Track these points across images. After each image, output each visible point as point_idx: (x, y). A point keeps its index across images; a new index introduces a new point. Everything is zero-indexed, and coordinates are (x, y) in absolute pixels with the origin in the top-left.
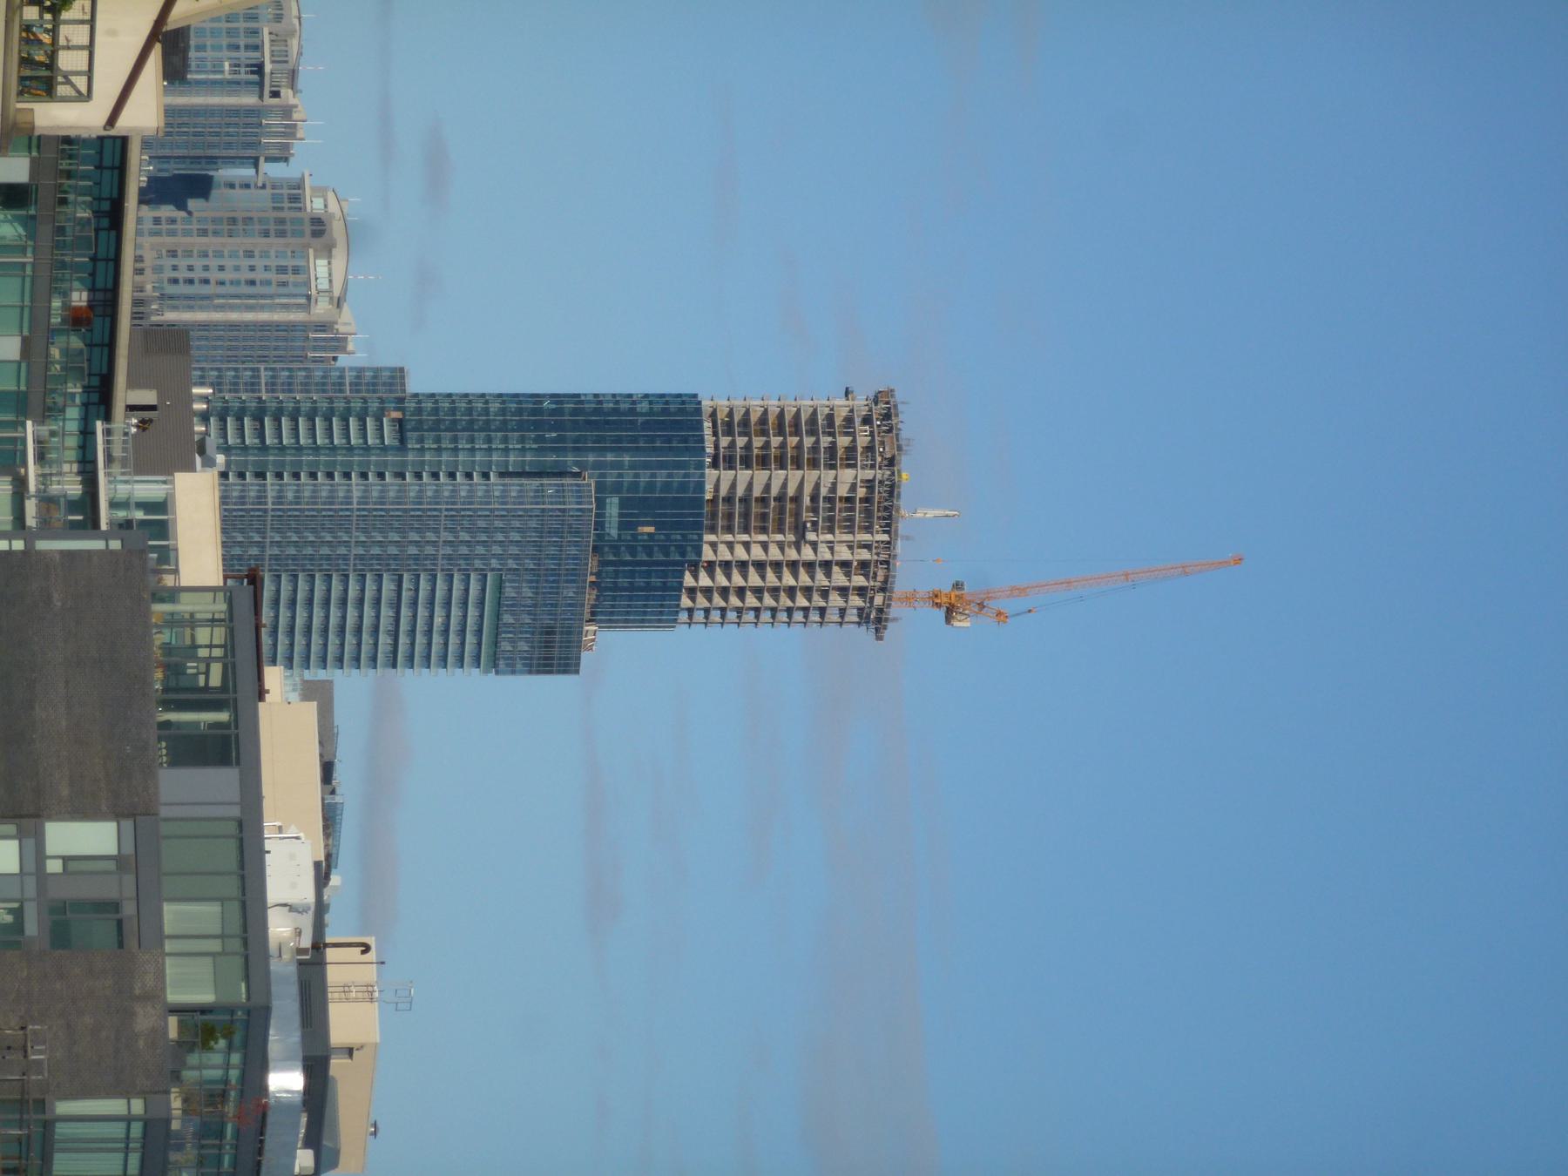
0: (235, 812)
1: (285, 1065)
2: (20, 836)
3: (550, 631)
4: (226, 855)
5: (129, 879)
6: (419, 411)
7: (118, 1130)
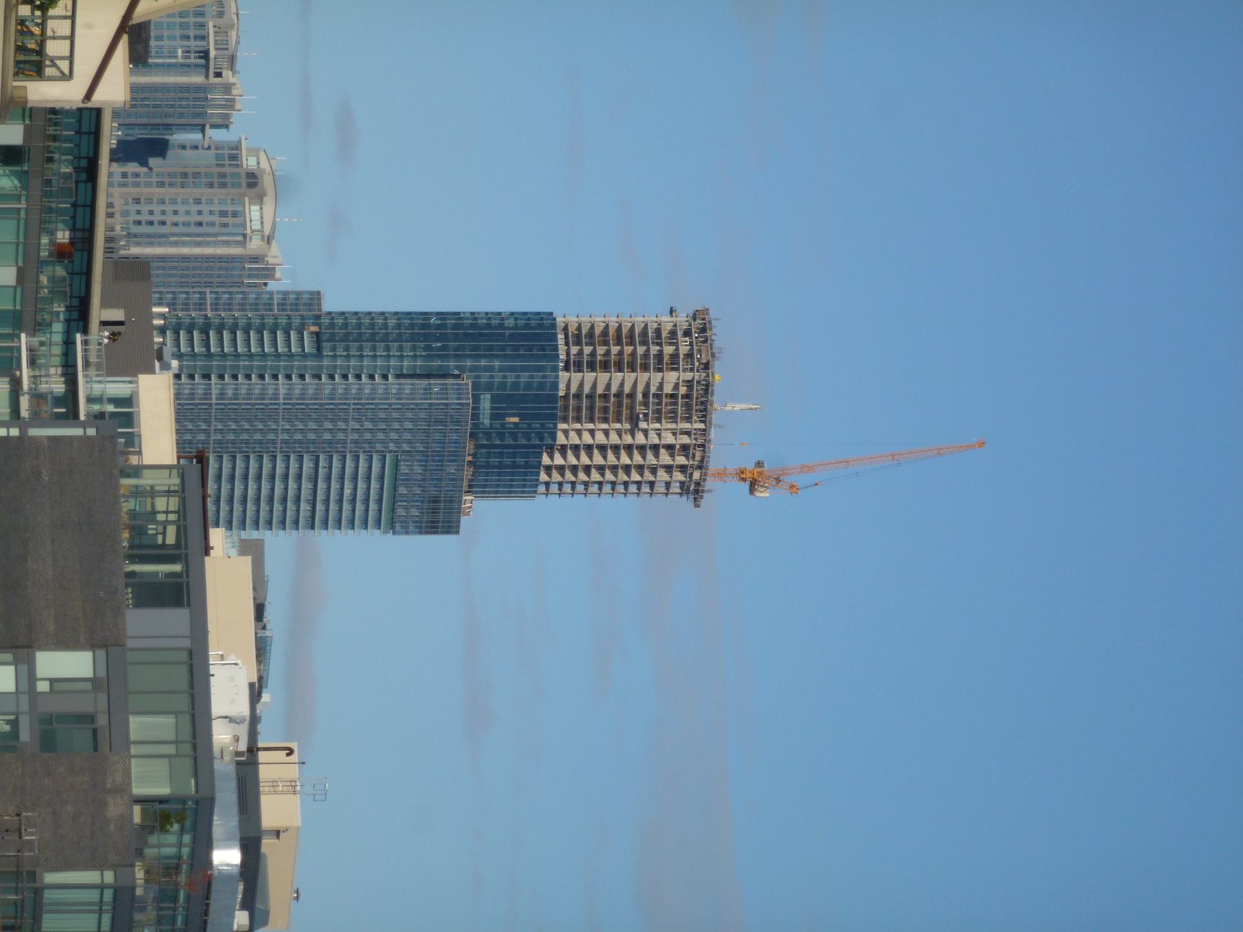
0: (186, 643)
1: (226, 844)
2: (16, 662)
3: (436, 500)
4: (179, 678)
5: (102, 697)
6: (332, 326)
7: (94, 895)
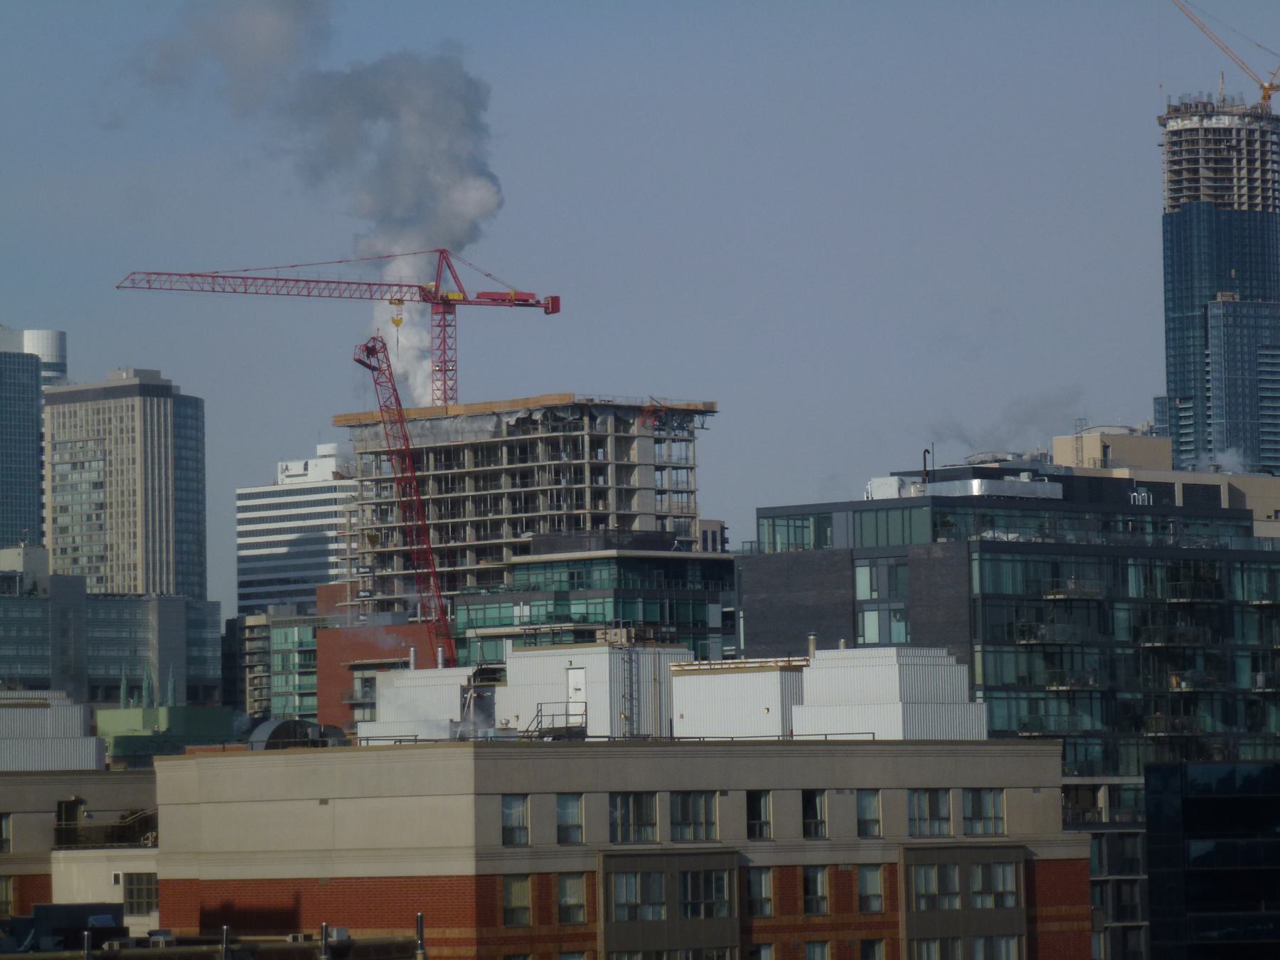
0: (850, 514)
2: (863, 612)
4: (869, 518)
5: (880, 561)
7: (987, 565)
